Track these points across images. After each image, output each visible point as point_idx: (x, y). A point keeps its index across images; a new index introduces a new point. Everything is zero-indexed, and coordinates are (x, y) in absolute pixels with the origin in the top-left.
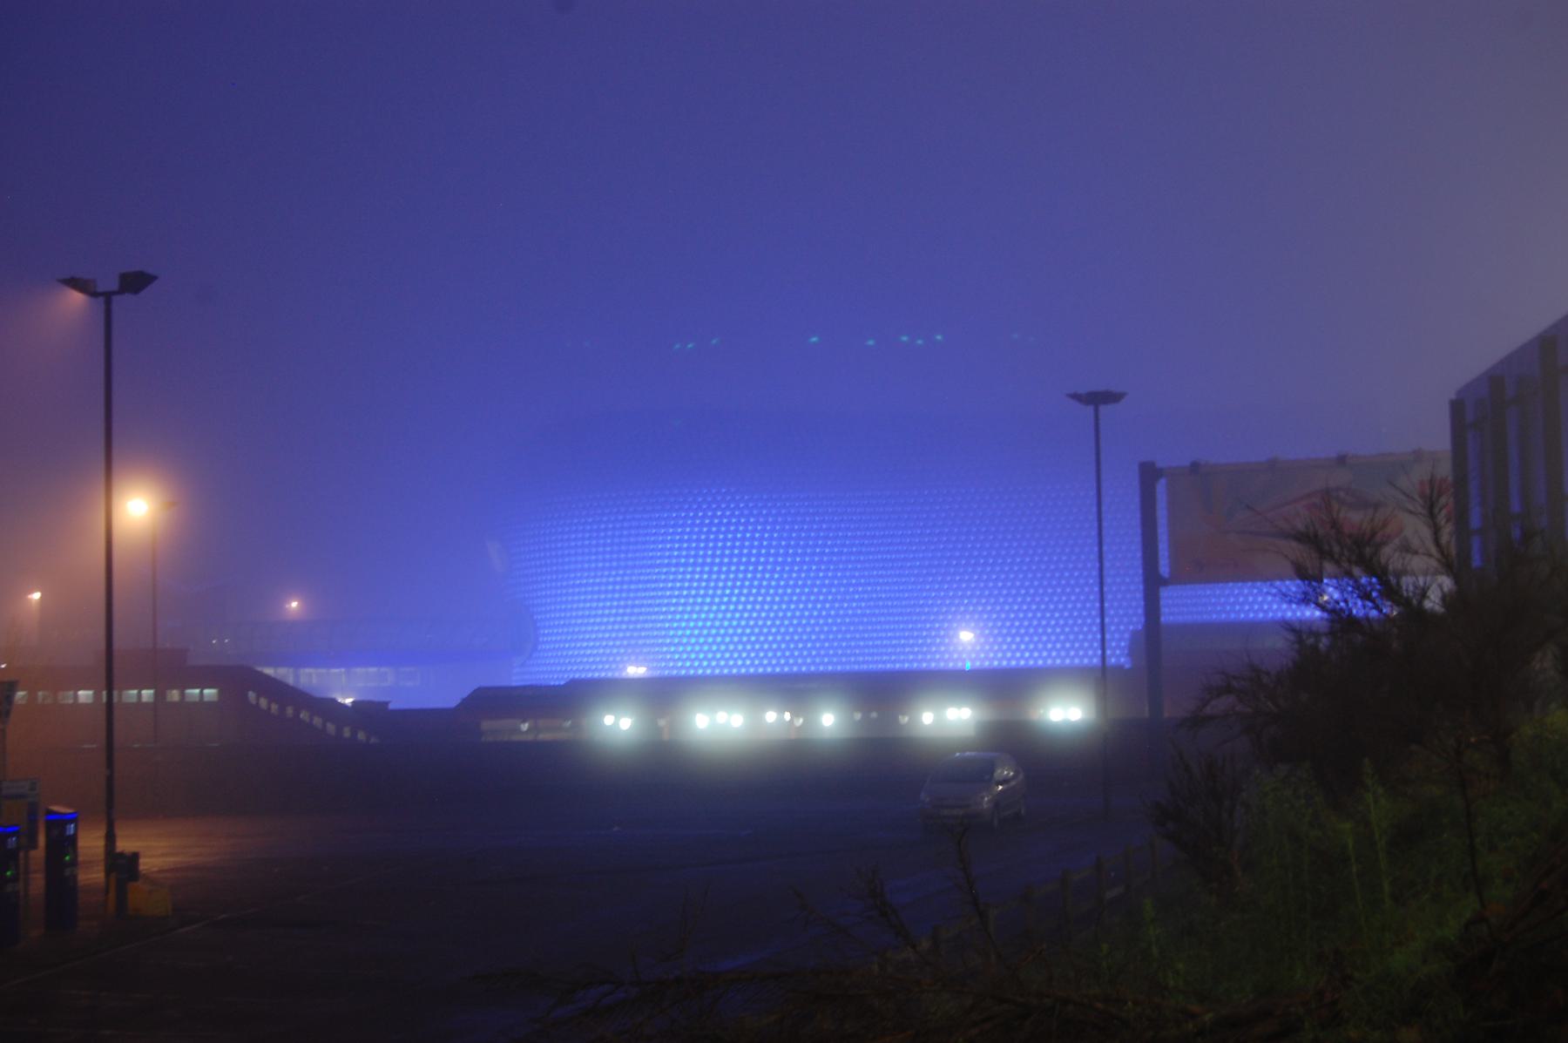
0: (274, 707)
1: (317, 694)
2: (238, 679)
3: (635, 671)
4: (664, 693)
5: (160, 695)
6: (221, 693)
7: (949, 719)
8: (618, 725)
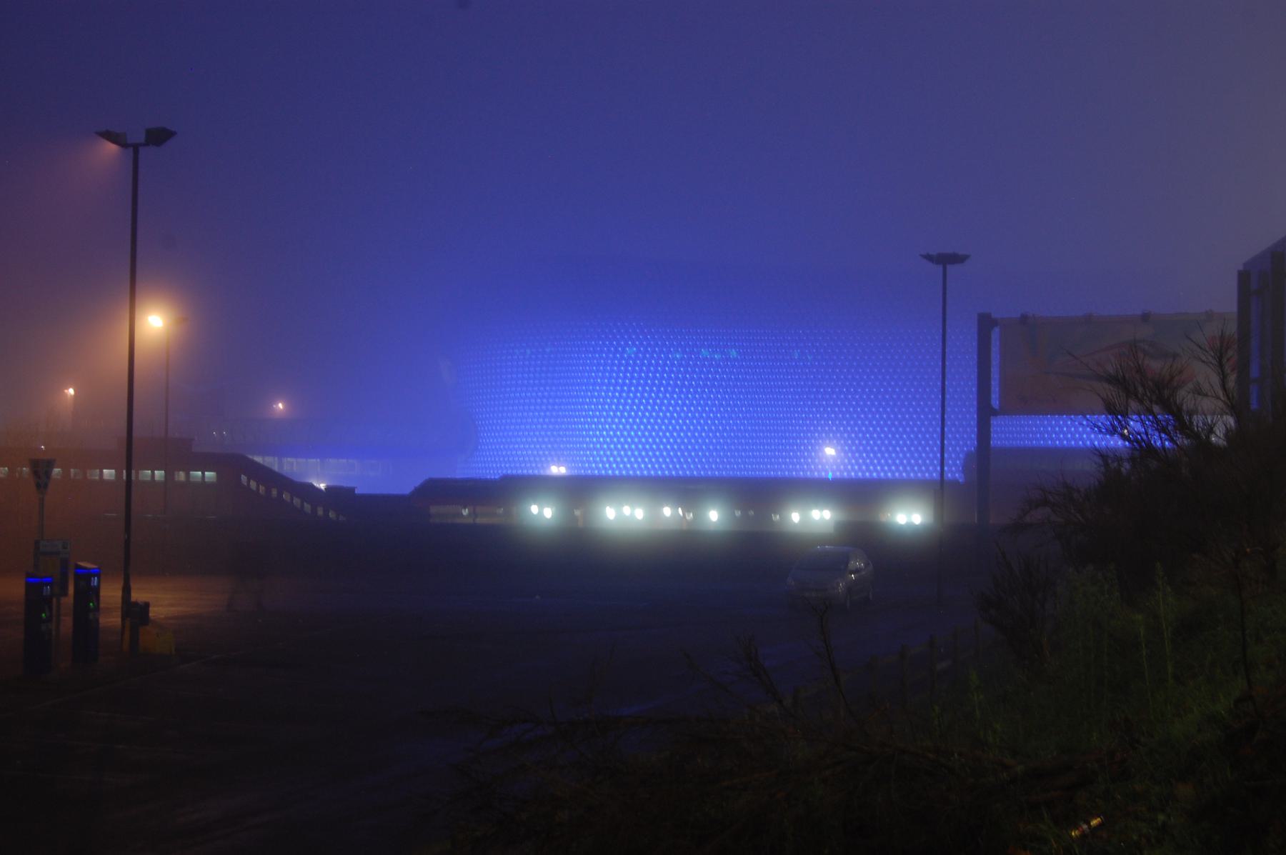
0: (262, 489)
3: (557, 470)
4: (579, 489)
7: (814, 518)
8: (542, 512)
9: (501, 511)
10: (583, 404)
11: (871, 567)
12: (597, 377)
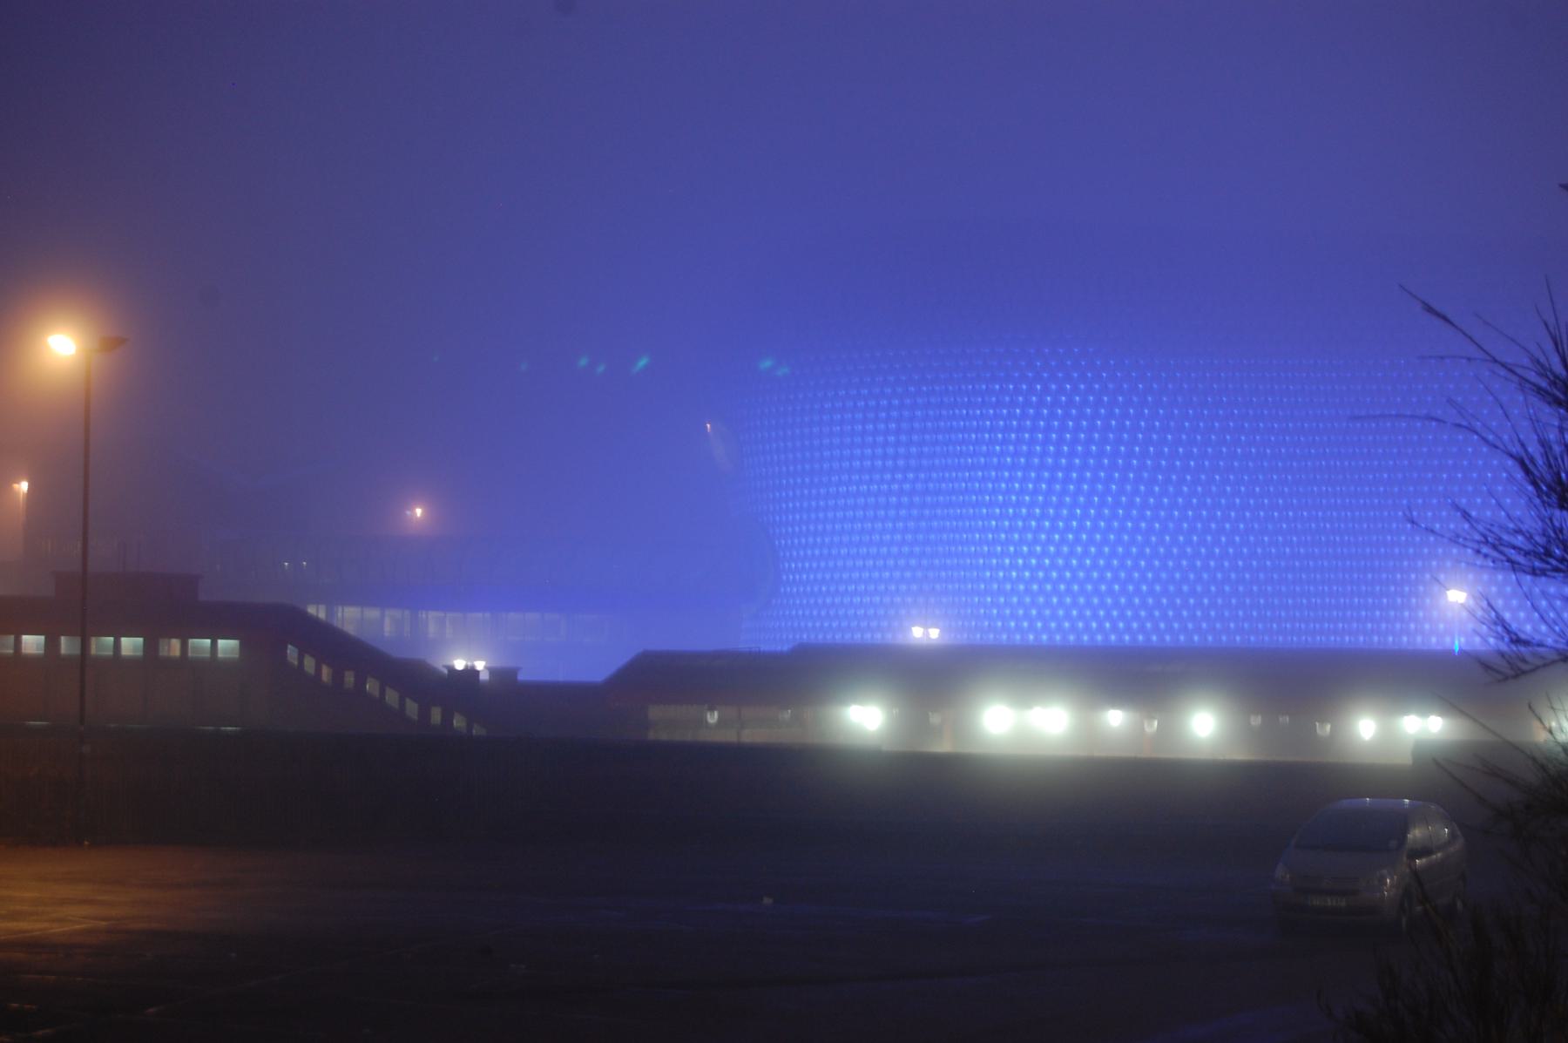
0: (326, 673)
1: (396, 653)
2: (273, 626)
3: (924, 633)
4: (931, 679)
5: (151, 646)
6: (242, 646)
7: (1397, 731)
8: (865, 719)
9: (787, 715)
10: (978, 505)
11: (1459, 844)
12: (1003, 454)
